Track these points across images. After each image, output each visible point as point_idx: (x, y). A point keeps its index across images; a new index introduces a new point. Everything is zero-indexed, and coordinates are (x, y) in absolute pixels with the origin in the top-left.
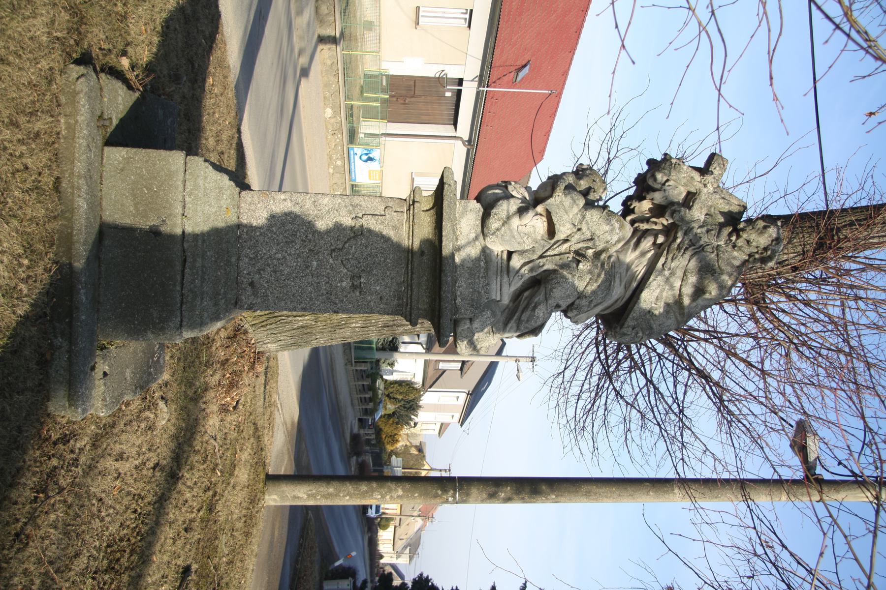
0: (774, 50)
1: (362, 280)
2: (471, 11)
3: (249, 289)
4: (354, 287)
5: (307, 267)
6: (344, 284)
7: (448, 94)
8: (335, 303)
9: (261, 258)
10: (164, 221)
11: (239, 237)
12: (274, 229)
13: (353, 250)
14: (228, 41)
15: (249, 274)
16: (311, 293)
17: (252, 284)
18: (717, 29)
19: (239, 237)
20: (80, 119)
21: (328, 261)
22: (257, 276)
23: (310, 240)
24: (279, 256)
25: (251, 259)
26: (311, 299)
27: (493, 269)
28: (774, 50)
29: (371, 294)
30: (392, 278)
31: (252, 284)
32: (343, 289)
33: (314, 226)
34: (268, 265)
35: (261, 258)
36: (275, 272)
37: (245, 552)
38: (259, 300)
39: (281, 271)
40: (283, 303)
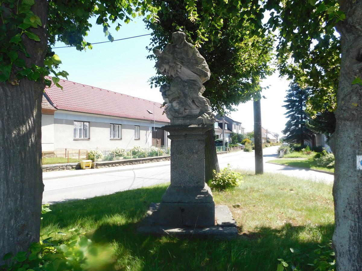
1: (195, 151)
2: (110, 124)
3: (198, 183)
6: (196, 156)
7: (156, 130)
10: (180, 208)
11: (184, 186)
12: (181, 177)
13: (186, 154)
15: (194, 184)
17: (197, 183)
18: (275, 165)
19: (184, 186)
21: (190, 161)
22: (195, 181)
26: (201, 166)
27: (251, 141)
31: (197, 183)
32: (198, 157)
33: (101, 226)
40: (202, 174)
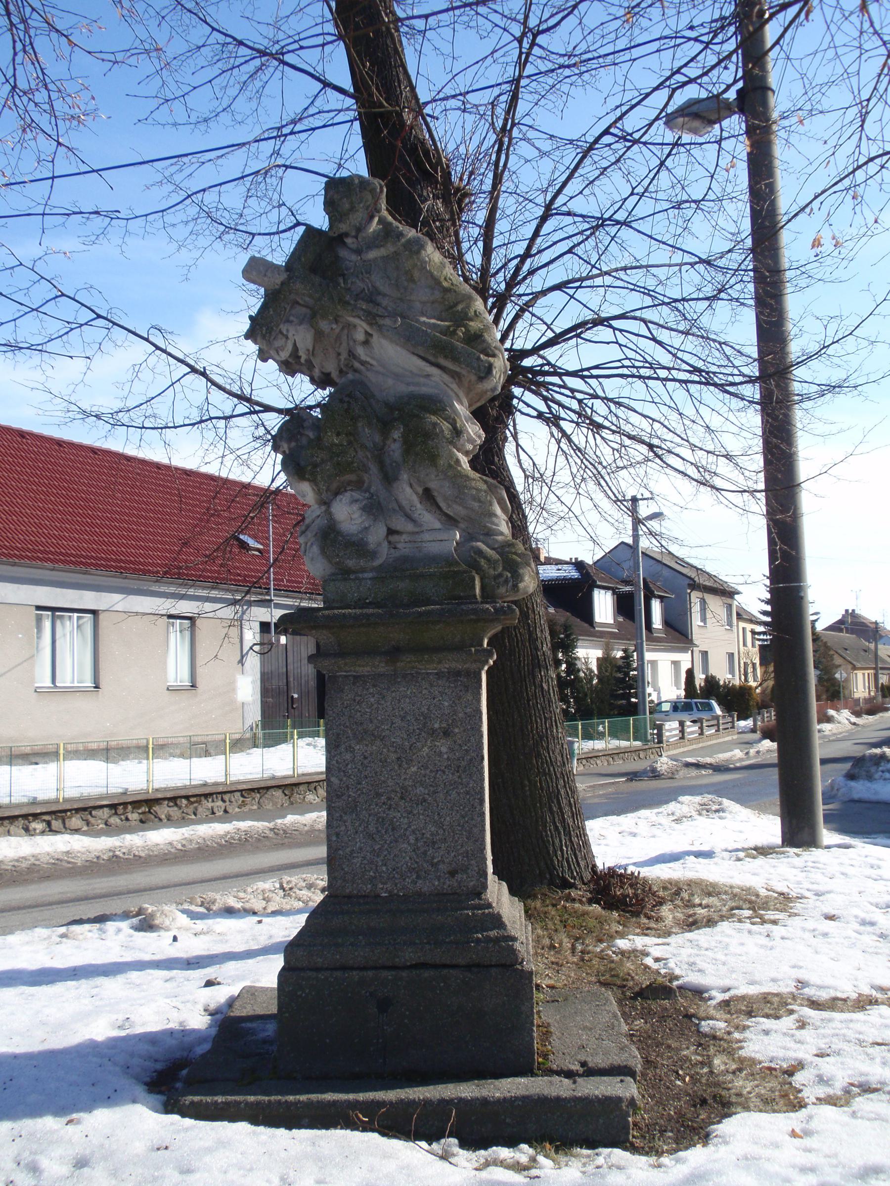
0: (477, 62)
2: (39, 608)
3: (459, 876)
4: (446, 733)
5: (425, 800)
6: (444, 749)
8: (471, 760)
9: (417, 862)
12: (377, 847)
14: (24, 933)
16: (459, 794)
17: (452, 873)
20: (220, 1101)
22: (441, 866)
23: (389, 799)
24: (412, 839)
25: (418, 877)
26: (467, 793)
28: (477, 62)
29: (455, 713)
30: (432, 685)
31: (452, 873)
32: (451, 750)
34: (425, 853)
35: (417, 862)
36: (434, 843)
37: (456, 884)
38: (473, 862)
39: (432, 835)
